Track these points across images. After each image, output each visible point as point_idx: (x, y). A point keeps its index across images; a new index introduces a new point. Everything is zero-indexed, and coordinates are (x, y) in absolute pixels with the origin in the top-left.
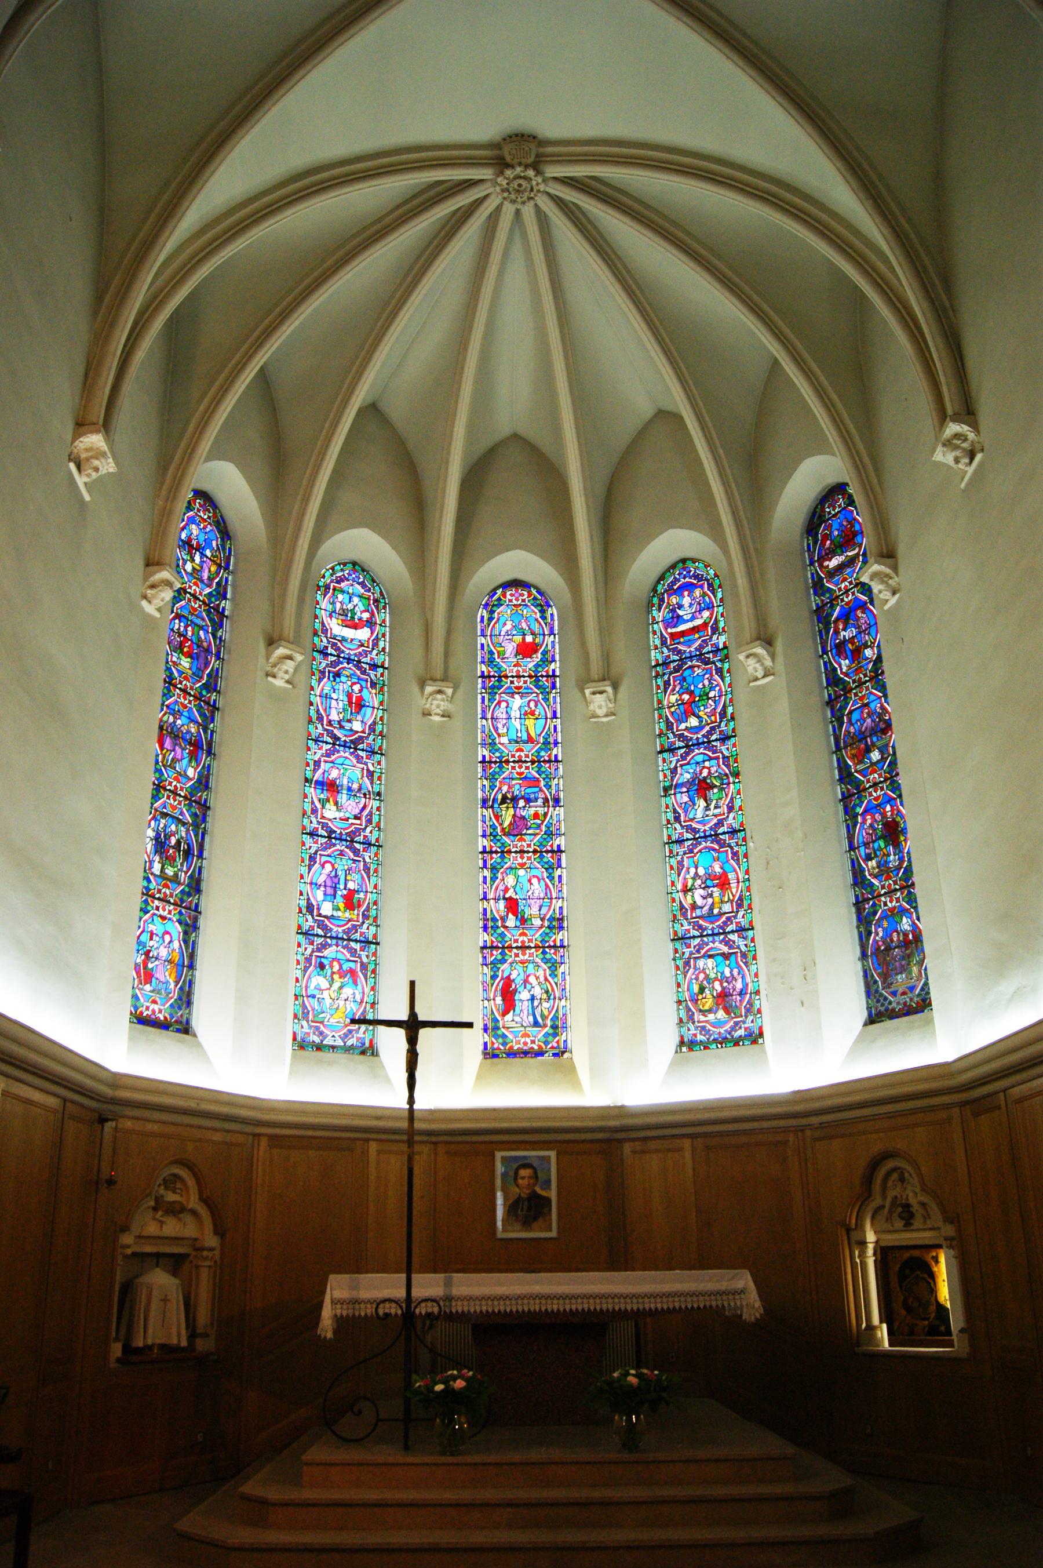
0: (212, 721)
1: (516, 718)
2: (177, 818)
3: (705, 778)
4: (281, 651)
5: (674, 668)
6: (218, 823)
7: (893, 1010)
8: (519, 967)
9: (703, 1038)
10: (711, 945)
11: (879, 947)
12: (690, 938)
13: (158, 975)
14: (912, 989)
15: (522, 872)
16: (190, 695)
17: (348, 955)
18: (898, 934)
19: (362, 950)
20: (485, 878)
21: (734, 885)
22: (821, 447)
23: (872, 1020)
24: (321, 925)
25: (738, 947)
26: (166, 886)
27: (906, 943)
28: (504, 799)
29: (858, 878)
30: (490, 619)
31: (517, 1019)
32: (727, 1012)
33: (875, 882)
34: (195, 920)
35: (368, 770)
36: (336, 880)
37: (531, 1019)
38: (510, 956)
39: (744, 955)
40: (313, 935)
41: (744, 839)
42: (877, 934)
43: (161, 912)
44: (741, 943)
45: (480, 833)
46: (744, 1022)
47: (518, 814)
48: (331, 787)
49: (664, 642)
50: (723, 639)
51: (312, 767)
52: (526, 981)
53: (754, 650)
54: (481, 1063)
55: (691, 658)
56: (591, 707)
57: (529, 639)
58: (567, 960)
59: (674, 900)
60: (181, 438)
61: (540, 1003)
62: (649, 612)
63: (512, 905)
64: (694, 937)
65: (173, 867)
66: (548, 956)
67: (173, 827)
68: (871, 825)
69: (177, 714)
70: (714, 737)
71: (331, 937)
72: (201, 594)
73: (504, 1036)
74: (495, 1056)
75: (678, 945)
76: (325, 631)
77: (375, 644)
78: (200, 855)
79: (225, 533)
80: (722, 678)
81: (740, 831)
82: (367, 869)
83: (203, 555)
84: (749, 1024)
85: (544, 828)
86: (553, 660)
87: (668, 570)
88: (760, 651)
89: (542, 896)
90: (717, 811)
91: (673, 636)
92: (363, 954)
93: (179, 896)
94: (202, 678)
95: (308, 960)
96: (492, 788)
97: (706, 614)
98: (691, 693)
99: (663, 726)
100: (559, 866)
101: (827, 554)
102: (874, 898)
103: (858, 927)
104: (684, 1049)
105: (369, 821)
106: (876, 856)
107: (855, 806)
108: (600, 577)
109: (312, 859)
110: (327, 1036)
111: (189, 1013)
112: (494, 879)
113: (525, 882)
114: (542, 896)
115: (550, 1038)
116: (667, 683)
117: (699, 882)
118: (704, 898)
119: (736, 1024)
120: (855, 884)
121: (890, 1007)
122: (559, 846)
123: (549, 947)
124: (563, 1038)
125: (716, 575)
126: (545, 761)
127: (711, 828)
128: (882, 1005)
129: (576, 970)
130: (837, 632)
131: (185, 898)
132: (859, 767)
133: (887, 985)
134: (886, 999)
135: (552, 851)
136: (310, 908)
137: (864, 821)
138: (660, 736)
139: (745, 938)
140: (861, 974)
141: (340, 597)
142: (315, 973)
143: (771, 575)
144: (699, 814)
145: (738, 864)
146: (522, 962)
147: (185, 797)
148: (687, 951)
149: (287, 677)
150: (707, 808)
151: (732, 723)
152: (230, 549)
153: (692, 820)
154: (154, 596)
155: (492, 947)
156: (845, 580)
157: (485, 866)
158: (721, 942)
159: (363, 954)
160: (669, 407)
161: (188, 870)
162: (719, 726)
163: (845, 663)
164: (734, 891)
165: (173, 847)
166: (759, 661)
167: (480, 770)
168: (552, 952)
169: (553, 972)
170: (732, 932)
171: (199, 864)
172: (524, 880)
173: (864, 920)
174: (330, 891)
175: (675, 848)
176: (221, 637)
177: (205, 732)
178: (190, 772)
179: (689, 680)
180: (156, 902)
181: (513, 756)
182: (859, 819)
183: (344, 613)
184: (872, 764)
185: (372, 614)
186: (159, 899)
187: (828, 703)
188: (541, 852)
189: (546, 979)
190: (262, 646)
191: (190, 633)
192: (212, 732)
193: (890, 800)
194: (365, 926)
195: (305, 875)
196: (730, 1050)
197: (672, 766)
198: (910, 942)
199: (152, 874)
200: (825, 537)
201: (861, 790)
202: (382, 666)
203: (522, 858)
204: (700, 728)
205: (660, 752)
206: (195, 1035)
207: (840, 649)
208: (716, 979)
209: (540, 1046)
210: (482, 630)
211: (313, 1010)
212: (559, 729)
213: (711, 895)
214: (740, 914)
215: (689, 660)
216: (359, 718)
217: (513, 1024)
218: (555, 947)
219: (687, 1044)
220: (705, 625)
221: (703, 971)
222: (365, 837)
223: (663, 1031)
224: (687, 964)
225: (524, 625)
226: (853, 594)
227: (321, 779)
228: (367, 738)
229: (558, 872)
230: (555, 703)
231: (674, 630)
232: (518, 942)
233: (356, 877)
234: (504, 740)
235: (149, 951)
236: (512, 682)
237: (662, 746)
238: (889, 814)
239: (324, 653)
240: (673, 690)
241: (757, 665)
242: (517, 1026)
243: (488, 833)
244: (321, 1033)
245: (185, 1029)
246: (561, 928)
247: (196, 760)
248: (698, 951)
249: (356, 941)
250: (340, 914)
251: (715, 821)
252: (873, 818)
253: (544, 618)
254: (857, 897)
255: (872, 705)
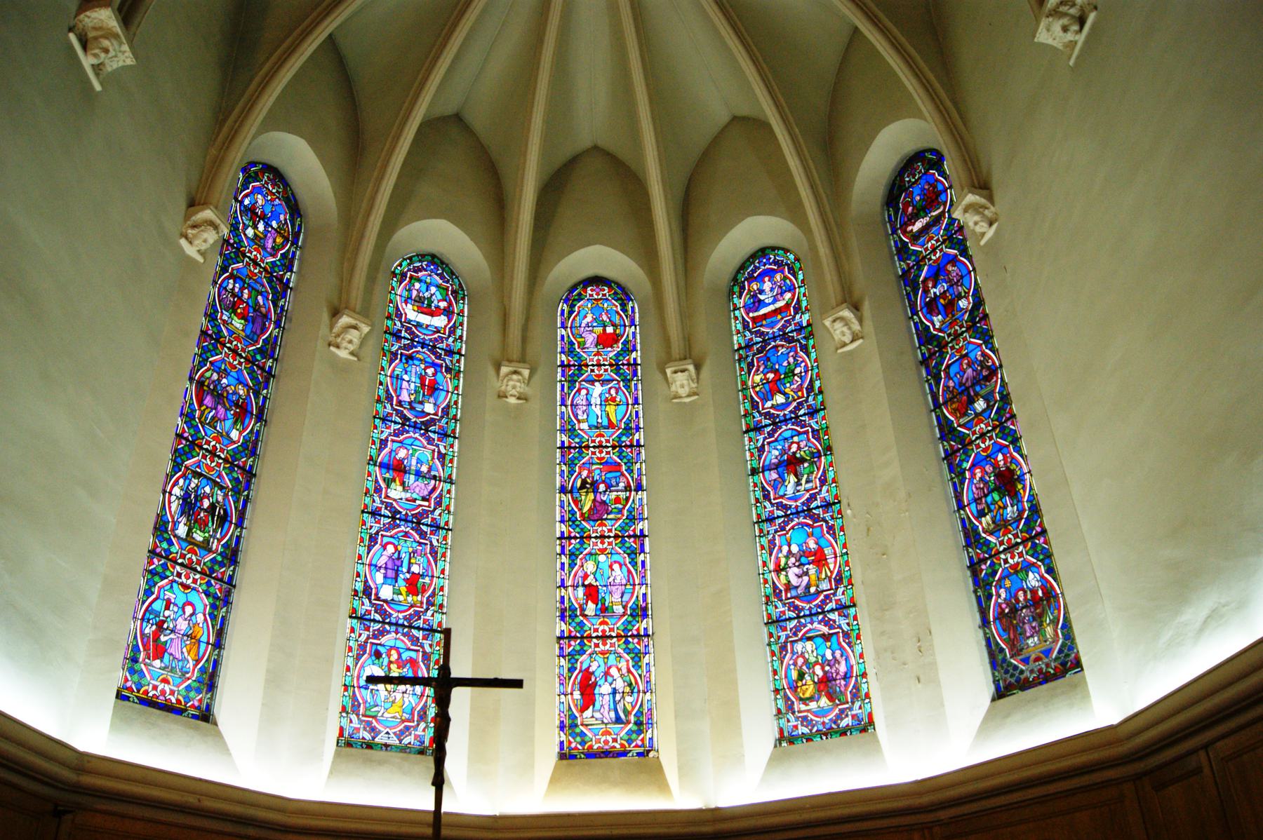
0: (266, 387)
1: (596, 404)
2: (215, 482)
3: (794, 453)
4: (345, 320)
5: (757, 351)
6: (262, 490)
7: (1027, 679)
8: (600, 658)
9: (806, 730)
10: (809, 626)
11: (1003, 610)
12: (786, 620)
13: (171, 650)
14: (1048, 652)
15: (602, 558)
16: (241, 357)
17: (409, 644)
18: (1025, 592)
19: (425, 638)
20: (563, 564)
21: (831, 561)
22: (899, 108)
23: (1000, 693)
24: (379, 610)
25: (840, 627)
26: (192, 551)
27: (1035, 602)
28: (583, 486)
29: (971, 538)
30: (571, 313)
31: (597, 715)
32: (831, 699)
33: (992, 539)
34: (228, 594)
35: (439, 452)
36: (398, 563)
37: (613, 714)
38: (590, 647)
39: (847, 635)
40: (370, 620)
41: (840, 512)
42: (999, 596)
43: (184, 580)
44: (843, 622)
45: (558, 518)
46: (850, 709)
47: (599, 497)
48: (399, 469)
49: (746, 326)
50: (806, 317)
51: (378, 445)
52: (607, 674)
53: (841, 314)
54: (555, 767)
55: (774, 339)
56: (673, 388)
57: (610, 330)
58: (652, 651)
59: (766, 581)
60: (242, 95)
61: (623, 697)
62: (730, 299)
63: (592, 593)
64: (790, 619)
65: (204, 532)
66: (631, 646)
67: (207, 489)
68: (982, 479)
69: (224, 373)
70: (802, 412)
71: (390, 624)
72: (262, 261)
73: (582, 734)
74: (573, 757)
75: (772, 629)
76: (399, 315)
77: (452, 332)
78: (240, 524)
79: (295, 209)
80: (808, 355)
81: (834, 503)
82: (434, 552)
83: (267, 225)
84: (856, 711)
85: (625, 513)
86: (634, 349)
87: (748, 260)
88: (846, 313)
89: (624, 582)
90: (809, 486)
91: (754, 319)
92: (426, 643)
93: (209, 564)
94: (257, 342)
95: (362, 647)
96: (571, 473)
97: (788, 296)
98: (776, 372)
99: (748, 406)
100: (642, 551)
101: (910, 220)
102: (991, 556)
103: (975, 592)
104: (784, 744)
105: (439, 504)
106: (990, 511)
107: (961, 461)
108: (680, 267)
109: (373, 539)
110: (380, 732)
111: (211, 698)
112: (572, 566)
113: (604, 567)
114: (624, 582)
115: (634, 736)
116: (751, 365)
117: (793, 560)
118: (799, 576)
119: (842, 711)
120: (968, 544)
121: (1022, 677)
122: (642, 531)
123: (633, 636)
124: (649, 735)
125: (797, 259)
126: (626, 446)
127: (803, 504)
128: (1012, 676)
129: (659, 663)
130: (926, 291)
131: (216, 567)
132: (962, 421)
133: (1016, 652)
134: (1016, 668)
135: (635, 536)
136: (367, 591)
137: (973, 476)
138: (745, 416)
139: (847, 616)
140: (984, 643)
141: (417, 285)
142: (370, 661)
143: (854, 243)
144: (790, 490)
145: (835, 538)
146: (603, 653)
147: (226, 460)
148: (783, 635)
149: (351, 347)
150: (798, 483)
151: (820, 397)
152: (300, 226)
153: (782, 497)
154: (195, 236)
155: (570, 637)
156: (931, 238)
157: (563, 552)
158: (819, 623)
159: (426, 643)
160: (744, 110)
161: (223, 538)
162: (807, 401)
163: (937, 320)
164: (831, 566)
165: (205, 511)
166: (846, 324)
167: (558, 455)
168: (635, 642)
169: (636, 663)
170: (832, 610)
171: (237, 533)
172: (605, 566)
173: (981, 585)
174: (390, 573)
175: (765, 526)
176: (282, 307)
177: (256, 397)
178: (234, 435)
179: (773, 359)
180: (178, 568)
181: (593, 441)
182: (967, 474)
183: (419, 300)
184: (977, 415)
185: (450, 304)
186: (182, 565)
187: (922, 363)
188: (623, 537)
189: (629, 671)
190: (325, 316)
191: (246, 296)
192: (265, 398)
193: (1001, 448)
194: (430, 613)
195: (364, 556)
196: (837, 740)
197: (759, 444)
198: (1041, 599)
199: (175, 536)
200: (906, 205)
201: (965, 444)
202: (459, 353)
203: (603, 543)
204: (787, 404)
205: (747, 432)
206: (216, 724)
207: (931, 307)
208: (816, 663)
209: (622, 746)
210: (562, 323)
211: (365, 702)
212: (641, 414)
213: (806, 573)
214: (840, 590)
215: (773, 347)
216: (432, 400)
217: (592, 721)
218: (638, 636)
219: (786, 738)
220: (788, 305)
221: (802, 655)
222: (433, 519)
223: (759, 724)
224: (783, 648)
225: (605, 318)
226: (941, 250)
227: (386, 460)
228: (439, 420)
229: (642, 557)
230: (636, 389)
231: (756, 314)
232: (601, 632)
233: (423, 560)
234: (584, 426)
235: (163, 622)
236: (592, 371)
237: (748, 425)
238: (1002, 463)
239: (397, 336)
240: (757, 370)
241: (845, 329)
242: (598, 724)
243: (566, 518)
244: (373, 729)
245: (206, 716)
246: (645, 616)
247: (243, 423)
248: (795, 634)
249: (419, 628)
250: (401, 598)
251: (807, 496)
252: (984, 471)
253: (625, 310)
254: (971, 559)
255: (972, 356)
